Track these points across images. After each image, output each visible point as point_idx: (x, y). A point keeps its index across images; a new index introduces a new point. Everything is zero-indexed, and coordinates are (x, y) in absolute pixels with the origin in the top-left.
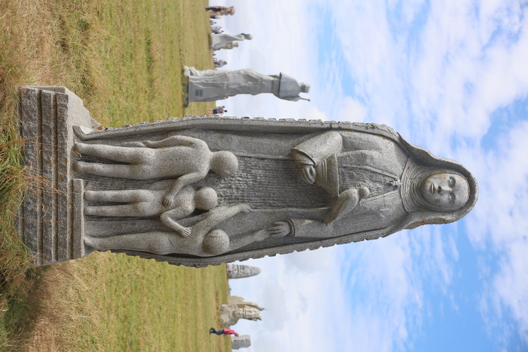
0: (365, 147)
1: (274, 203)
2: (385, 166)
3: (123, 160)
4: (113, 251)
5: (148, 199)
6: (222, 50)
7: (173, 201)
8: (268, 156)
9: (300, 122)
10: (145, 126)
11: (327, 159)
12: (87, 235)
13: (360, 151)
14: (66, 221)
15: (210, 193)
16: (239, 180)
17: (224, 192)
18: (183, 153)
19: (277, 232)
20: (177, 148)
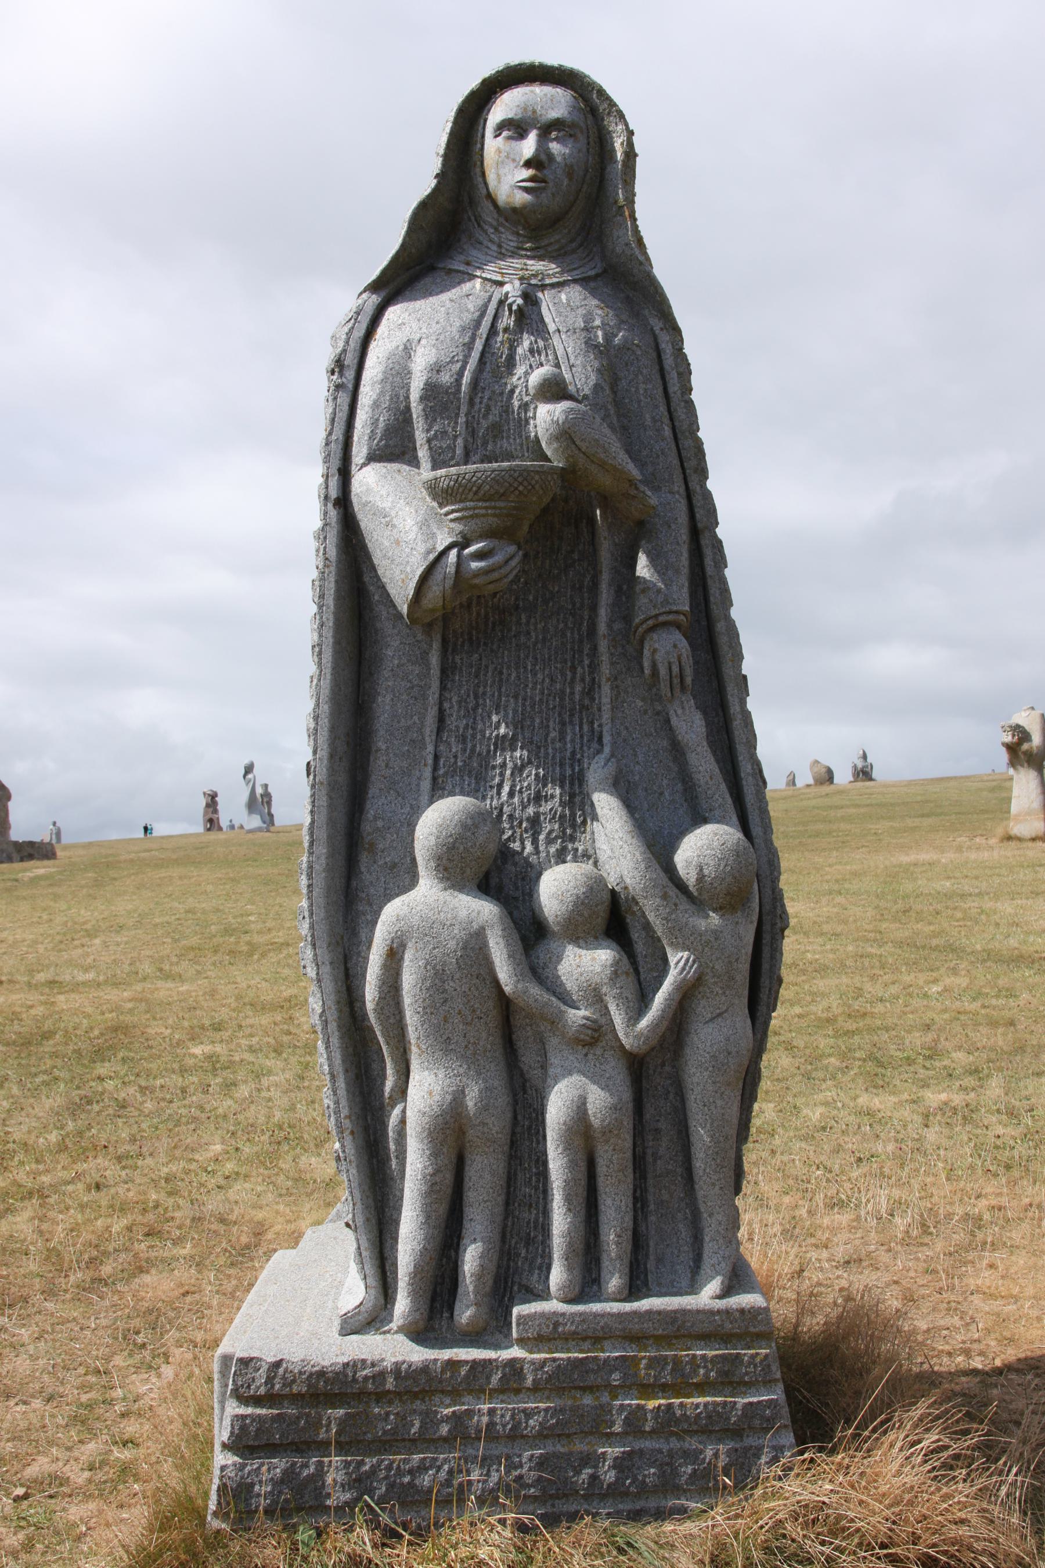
0: (402, 392)
1: (583, 680)
2: (463, 329)
3: (449, 1177)
4: (737, 1190)
5: (576, 1093)
6: (273, 811)
7: (582, 1013)
8: (433, 696)
9: (322, 596)
10: (337, 1103)
11: (441, 505)
12: (693, 1289)
13: (413, 405)
14: (650, 1358)
15: (556, 888)
16: (511, 794)
17: (549, 841)
18: (424, 980)
19: (675, 669)
20: (407, 1000)
